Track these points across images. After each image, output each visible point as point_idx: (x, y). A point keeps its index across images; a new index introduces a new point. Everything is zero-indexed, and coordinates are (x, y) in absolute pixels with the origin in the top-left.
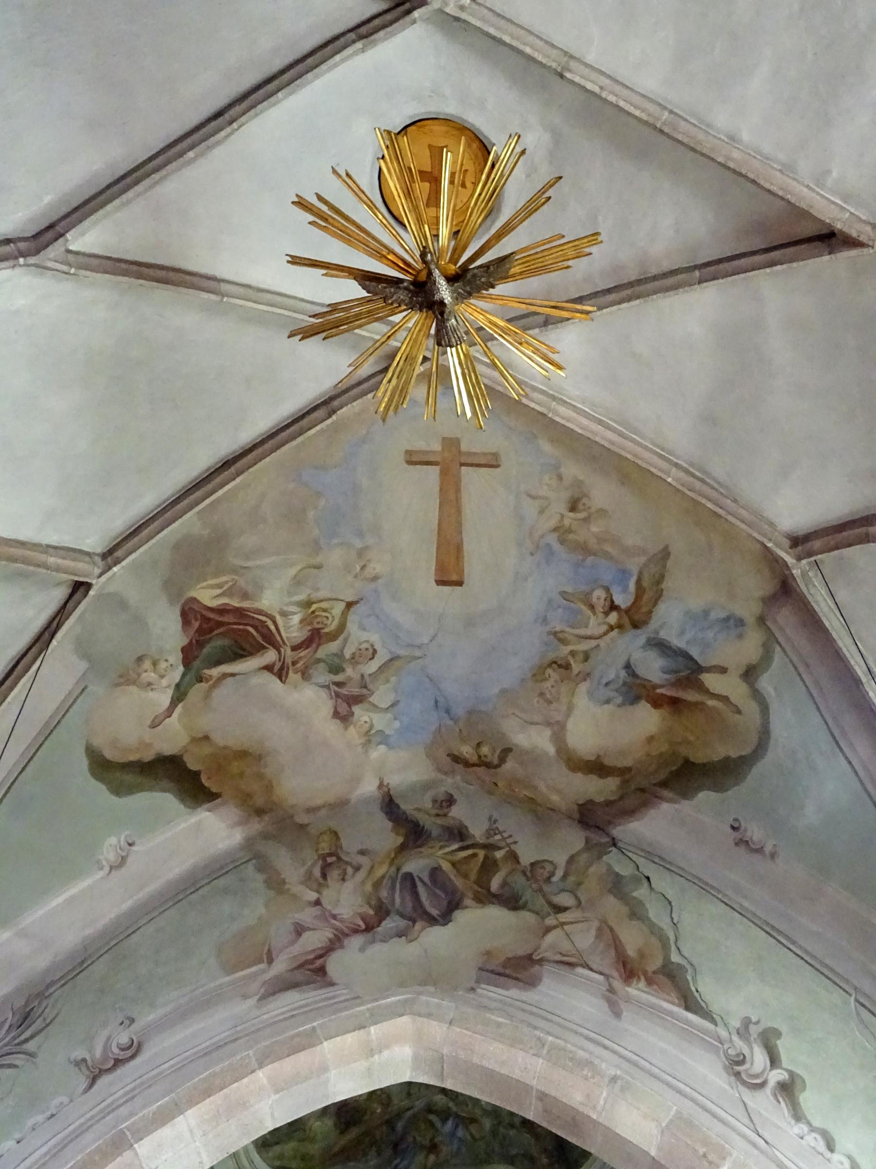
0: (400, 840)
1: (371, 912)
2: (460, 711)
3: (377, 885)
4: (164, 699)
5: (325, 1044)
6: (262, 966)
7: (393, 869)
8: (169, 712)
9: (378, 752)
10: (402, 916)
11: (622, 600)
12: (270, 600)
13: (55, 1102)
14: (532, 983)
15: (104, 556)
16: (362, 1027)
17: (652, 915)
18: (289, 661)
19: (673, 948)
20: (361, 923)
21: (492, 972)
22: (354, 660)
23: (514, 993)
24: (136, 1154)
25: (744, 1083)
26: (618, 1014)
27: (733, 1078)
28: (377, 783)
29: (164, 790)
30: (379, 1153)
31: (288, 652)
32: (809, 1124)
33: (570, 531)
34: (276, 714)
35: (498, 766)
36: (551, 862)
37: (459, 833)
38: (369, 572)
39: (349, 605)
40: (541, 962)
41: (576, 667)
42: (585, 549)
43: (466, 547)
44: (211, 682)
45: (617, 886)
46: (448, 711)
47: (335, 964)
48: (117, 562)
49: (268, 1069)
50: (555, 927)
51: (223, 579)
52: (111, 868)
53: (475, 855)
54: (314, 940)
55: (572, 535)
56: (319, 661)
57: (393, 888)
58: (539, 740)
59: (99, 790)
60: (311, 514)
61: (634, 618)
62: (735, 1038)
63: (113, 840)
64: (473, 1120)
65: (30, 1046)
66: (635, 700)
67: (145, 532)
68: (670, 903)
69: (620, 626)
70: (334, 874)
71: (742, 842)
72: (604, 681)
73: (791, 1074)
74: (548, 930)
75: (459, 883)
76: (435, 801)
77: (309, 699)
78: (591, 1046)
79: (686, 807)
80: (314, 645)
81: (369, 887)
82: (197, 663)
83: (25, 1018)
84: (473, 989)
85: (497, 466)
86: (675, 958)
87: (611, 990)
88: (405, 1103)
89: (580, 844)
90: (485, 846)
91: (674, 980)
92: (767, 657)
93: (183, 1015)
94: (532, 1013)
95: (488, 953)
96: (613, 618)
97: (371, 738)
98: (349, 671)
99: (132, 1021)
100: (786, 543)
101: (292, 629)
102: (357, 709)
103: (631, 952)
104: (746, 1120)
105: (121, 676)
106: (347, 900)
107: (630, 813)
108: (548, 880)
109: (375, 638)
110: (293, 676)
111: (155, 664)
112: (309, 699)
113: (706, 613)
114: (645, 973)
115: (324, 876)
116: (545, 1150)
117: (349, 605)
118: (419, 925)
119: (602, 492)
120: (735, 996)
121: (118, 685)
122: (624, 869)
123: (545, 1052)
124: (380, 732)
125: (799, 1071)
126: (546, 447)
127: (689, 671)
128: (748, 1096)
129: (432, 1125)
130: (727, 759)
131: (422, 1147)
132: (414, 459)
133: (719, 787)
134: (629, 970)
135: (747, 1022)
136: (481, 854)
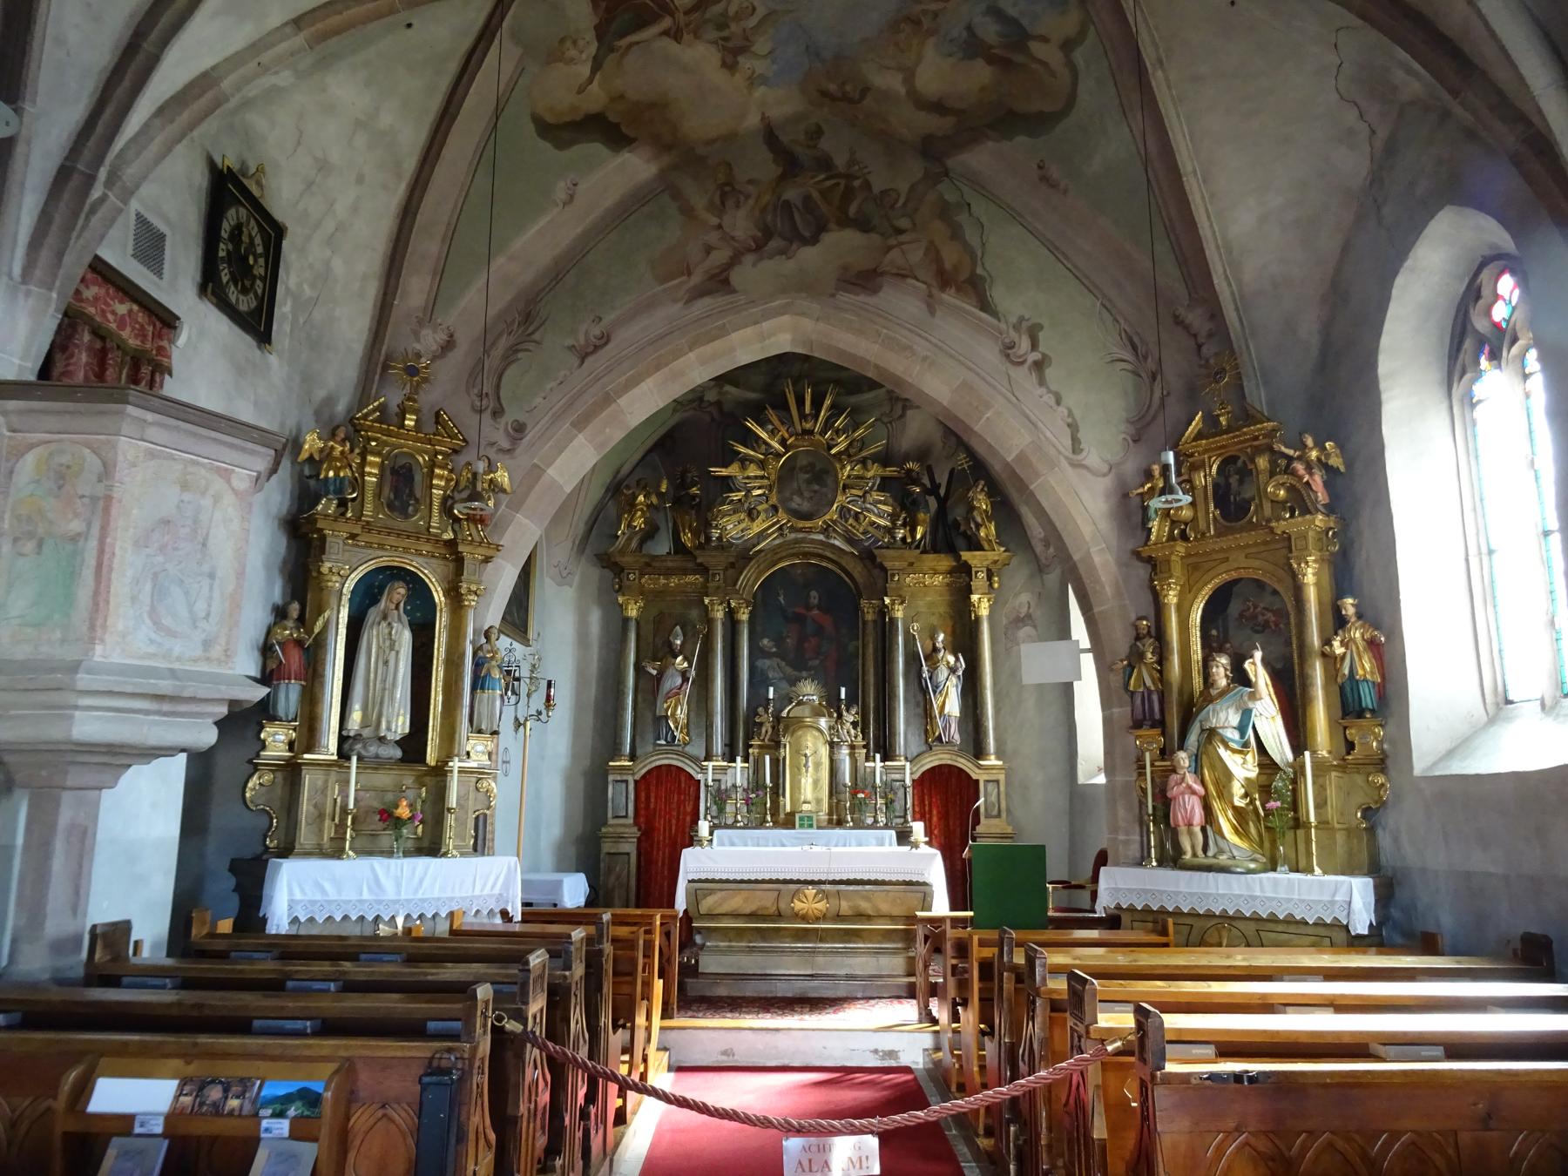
0: (780, 170)
3: (763, 210)
4: (586, 70)
9: (760, 92)
14: (875, 291)
16: (756, 323)
18: (682, 24)
22: (738, 17)
23: (862, 298)
26: (932, 313)
31: (681, 17)
37: (825, 164)
40: (883, 274)
41: (927, 23)
47: (736, 277)
54: (720, 256)
58: (891, 82)
62: (1012, 332)
63: (562, 184)
65: (536, 336)
70: (730, 203)
71: (1045, 179)
73: (1044, 355)
74: (890, 248)
83: (528, 318)
84: (833, 296)
86: (979, 271)
87: (930, 296)
91: (976, 289)
92: (1082, 34)
95: (845, 268)
97: (753, 81)
98: (734, 27)
102: (741, 59)
103: (948, 266)
106: (741, 224)
108: (892, 207)
111: (575, 42)
112: (701, 54)
115: (723, 203)
118: (794, 246)
122: (951, 197)
124: (761, 75)
127: (1018, 36)
134: (945, 279)
135: (1021, 319)
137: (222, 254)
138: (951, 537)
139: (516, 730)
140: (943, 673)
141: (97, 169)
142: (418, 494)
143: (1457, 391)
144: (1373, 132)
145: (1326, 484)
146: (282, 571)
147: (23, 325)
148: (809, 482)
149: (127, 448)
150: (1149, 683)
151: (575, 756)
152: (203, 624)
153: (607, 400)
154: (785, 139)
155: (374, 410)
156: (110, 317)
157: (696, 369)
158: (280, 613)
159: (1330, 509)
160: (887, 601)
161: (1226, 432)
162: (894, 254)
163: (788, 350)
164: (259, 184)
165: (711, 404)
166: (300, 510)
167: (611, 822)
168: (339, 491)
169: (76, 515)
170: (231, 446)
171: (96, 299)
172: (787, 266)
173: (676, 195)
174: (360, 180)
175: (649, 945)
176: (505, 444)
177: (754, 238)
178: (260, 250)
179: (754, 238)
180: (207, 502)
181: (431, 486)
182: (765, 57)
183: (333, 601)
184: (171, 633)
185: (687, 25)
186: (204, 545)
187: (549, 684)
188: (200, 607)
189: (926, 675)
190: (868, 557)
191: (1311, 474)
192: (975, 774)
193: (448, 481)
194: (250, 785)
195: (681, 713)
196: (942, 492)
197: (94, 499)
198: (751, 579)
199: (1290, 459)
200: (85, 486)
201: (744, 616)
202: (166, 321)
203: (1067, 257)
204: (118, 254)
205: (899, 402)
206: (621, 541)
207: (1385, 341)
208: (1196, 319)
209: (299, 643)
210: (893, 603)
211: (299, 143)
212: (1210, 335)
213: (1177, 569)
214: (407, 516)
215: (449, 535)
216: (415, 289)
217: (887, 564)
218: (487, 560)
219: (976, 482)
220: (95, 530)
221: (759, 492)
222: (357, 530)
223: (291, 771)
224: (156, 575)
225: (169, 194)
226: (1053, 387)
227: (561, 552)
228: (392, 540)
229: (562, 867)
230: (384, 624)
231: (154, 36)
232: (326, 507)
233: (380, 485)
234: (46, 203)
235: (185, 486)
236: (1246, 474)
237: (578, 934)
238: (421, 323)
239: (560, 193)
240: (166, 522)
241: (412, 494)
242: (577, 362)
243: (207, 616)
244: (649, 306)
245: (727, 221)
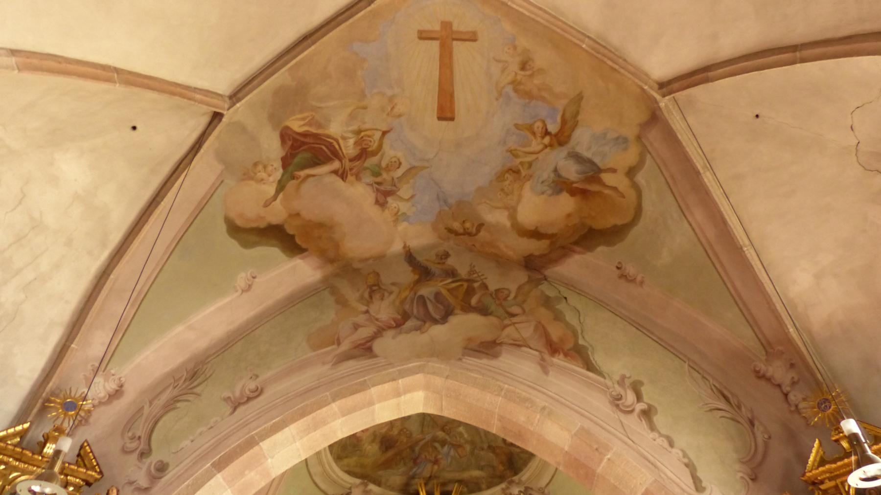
0: (417, 277)
1: (399, 317)
2: (452, 201)
3: (402, 302)
4: (271, 190)
5: (372, 389)
6: (334, 347)
7: (412, 293)
9: (403, 226)
10: (418, 319)
11: (553, 128)
12: (335, 127)
13: (215, 419)
14: (495, 356)
15: (230, 97)
16: (394, 380)
17: (568, 318)
18: (347, 168)
19: (580, 337)
20: (393, 323)
21: (471, 350)
22: (388, 169)
23: (485, 361)
24: (261, 449)
25: (621, 410)
26: (546, 373)
27: (615, 408)
28: (402, 245)
29: (273, 246)
30: (405, 464)
32: (659, 433)
33: (520, 83)
34: (341, 201)
35: (476, 235)
36: (507, 289)
37: (452, 273)
38: (396, 110)
39: (384, 133)
40: (501, 344)
41: (524, 172)
42: (529, 95)
43: (456, 93)
44: (300, 180)
45: (547, 302)
46: (445, 201)
47: (378, 346)
48: (239, 100)
49: (338, 403)
50: (510, 325)
51: (306, 114)
52: (243, 291)
53: (462, 285)
54: (365, 332)
55: (523, 84)
56: (366, 169)
57: (412, 303)
59: (233, 245)
60: (359, 73)
61: (560, 139)
62: (616, 386)
63: (243, 275)
64: (460, 446)
65: (198, 390)
66: (559, 192)
67: (255, 82)
68: (579, 312)
69: (551, 145)
70: (377, 296)
71: (623, 276)
72: (540, 181)
73: (649, 405)
74: (505, 327)
75: (451, 300)
76: (437, 255)
77: (360, 192)
78: (531, 391)
79: (589, 257)
80: (363, 159)
81: (397, 303)
82: (290, 168)
84: (460, 359)
85: (475, 40)
86: (581, 342)
87: (543, 359)
88: (420, 436)
90: (468, 281)
93: (288, 372)
94: (495, 372)
95: (470, 340)
96: (547, 140)
97: (398, 217)
98: (385, 175)
99: (257, 376)
100: (656, 86)
101: (349, 148)
102: (389, 199)
104: (622, 431)
105: (244, 174)
106: (384, 310)
107: (555, 261)
108: (505, 299)
109: (400, 155)
110: (350, 178)
111: (265, 167)
112: (360, 192)
113: (605, 134)
114: (563, 350)
115: (371, 297)
116: (501, 463)
117: (384, 133)
118: (427, 325)
119: (543, 57)
120: (615, 365)
121: (243, 180)
122: (551, 293)
123: (503, 393)
124: (404, 214)
125: (656, 405)
126: (507, 26)
128: (623, 417)
129: (436, 448)
130: (615, 226)
131: (430, 461)
132: (424, 35)
133: (610, 244)
134: (554, 348)
135: (623, 377)
136: (465, 285)
153: (251, 443)
154: (420, 259)
155: (15, 435)
163: (421, 410)
172: (421, 339)
174: (69, 243)
176: (143, 482)
182: (408, 200)
185: (351, 169)
203: (652, 333)
208: (778, 371)
211: (20, 203)
212: (794, 383)
216: (95, 342)
239: (241, 279)
242: (228, 409)
244: (303, 366)
245: (373, 309)
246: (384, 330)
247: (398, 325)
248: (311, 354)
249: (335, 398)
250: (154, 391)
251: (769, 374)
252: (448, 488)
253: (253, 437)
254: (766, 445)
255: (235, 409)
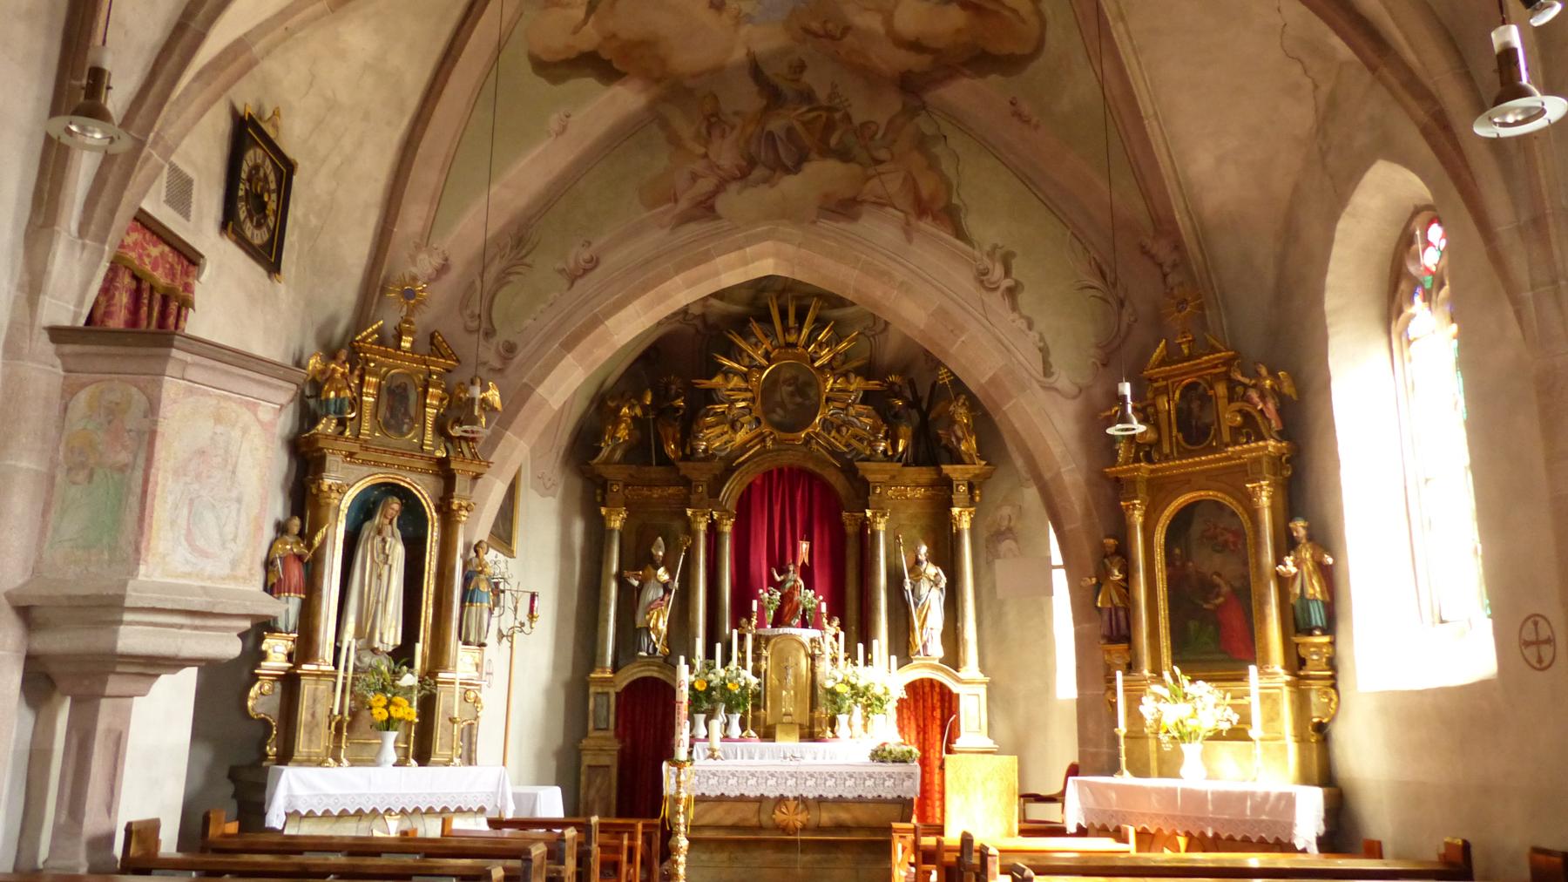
0: (765, 102)
4: (580, 13)
8: (585, 22)
9: (745, 30)
14: (854, 218)
16: (740, 248)
23: (842, 225)
26: (910, 240)
37: (807, 96)
40: (862, 202)
47: (721, 204)
49: (682, 275)
54: (706, 185)
58: (870, 22)
59: (542, 84)
65: (528, 260)
70: (716, 132)
71: (1018, 115)
73: (1017, 283)
74: (869, 178)
79: (978, 83)
84: (814, 222)
86: (955, 201)
87: (908, 224)
89: (898, 107)
95: (826, 196)
103: (925, 194)
106: (726, 154)
108: (872, 138)
115: (709, 133)
120: (987, 231)
128: (986, 296)
134: (922, 208)
135: (995, 247)
137: (241, 193)
138: (931, 451)
139: (499, 642)
140: (924, 587)
141: (147, 135)
142: (412, 412)
143: (1396, 328)
144: (1316, 87)
145: (1280, 411)
146: (283, 487)
147: (266, 412)
148: (792, 394)
149: (171, 387)
150: (1116, 600)
151: (556, 667)
152: (231, 545)
153: (596, 322)
154: (768, 72)
156: (147, 260)
157: (683, 292)
158: (281, 529)
159: (1282, 435)
160: (869, 513)
161: (1189, 359)
162: (875, 182)
164: (275, 127)
165: (696, 317)
166: (302, 430)
167: (592, 734)
168: (340, 411)
169: (124, 447)
170: (259, 382)
171: (135, 244)
173: (664, 124)
175: (631, 850)
176: (497, 364)
177: (739, 168)
178: (273, 186)
179: (739, 168)
180: (236, 433)
181: (425, 406)
183: (331, 516)
184: (204, 554)
186: (234, 472)
187: (533, 596)
188: (229, 530)
189: (908, 587)
190: (849, 469)
191: (1265, 403)
192: (955, 687)
193: (442, 400)
194: (252, 693)
195: (663, 626)
196: (924, 406)
197: (140, 433)
198: (731, 491)
199: (1246, 387)
200: (133, 420)
201: (727, 528)
202: (190, 259)
204: (156, 206)
205: (876, 325)
206: (605, 453)
207: (1330, 279)
208: (1162, 250)
209: (300, 558)
210: (874, 515)
212: (1175, 266)
213: (1142, 488)
214: (403, 434)
215: (441, 454)
217: (870, 478)
218: (476, 477)
219: (957, 399)
220: (141, 462)
221: (742, 404)
222: (355, 448)
223: (290, 683)
224: (191, 501)
225: (200, 150)
226: (1025, 312)
227: (552, 466)
228: (387, 458)
229: (541, 781)
230: (378, 539)
231: (201, 16)
232: (327, 426)
233: (377, 403)
234: (101, 167)
235: (218, 420)
236: (1207, 400)
237: (570, 833)
238: (418, 247)
239: (554, 122)
240: (202, 452)
241: (406, 413)
242: (564, 283)
243: (234, 539)
246: (727, 182)
247: (743, 175)
248: (645, 215)
249: (680, 268)
250: (483, 259)
251: (1154, 251)
252: (805, 302)
253: (596, 315)
254: (1129, 326)
255: (572, 284)
